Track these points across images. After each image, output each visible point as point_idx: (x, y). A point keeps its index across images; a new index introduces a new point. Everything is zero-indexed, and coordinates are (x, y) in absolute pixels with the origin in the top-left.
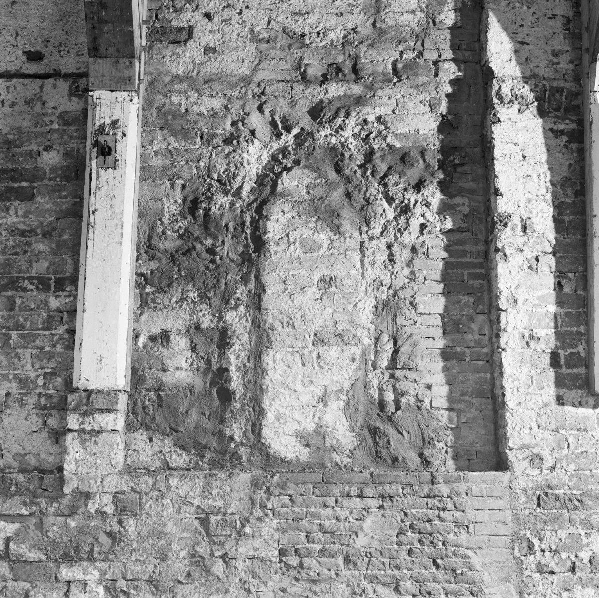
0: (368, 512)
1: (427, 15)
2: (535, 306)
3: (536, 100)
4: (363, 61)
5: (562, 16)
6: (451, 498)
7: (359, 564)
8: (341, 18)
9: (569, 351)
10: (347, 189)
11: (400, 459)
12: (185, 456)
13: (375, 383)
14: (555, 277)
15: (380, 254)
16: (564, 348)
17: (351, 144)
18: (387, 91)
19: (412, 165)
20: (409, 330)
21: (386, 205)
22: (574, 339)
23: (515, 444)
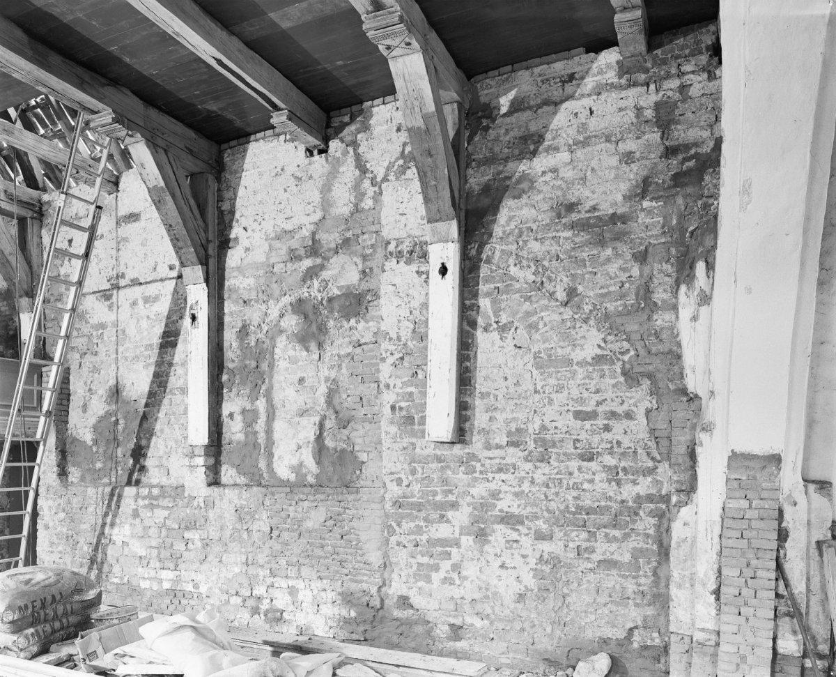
12: (243, 479)
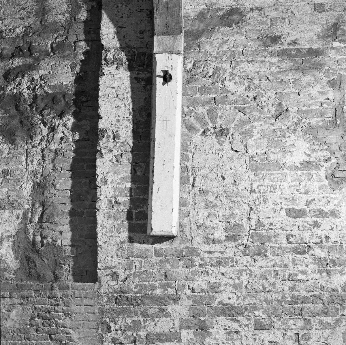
0: (14, 307)
1: (71, 16)
2: (119, 184)
3: (128, 61)
4: (34, 44)
5: (147, 10)
6: (62, 299)
7: (7, 337)
8: (22, 20)
9: (138, 210)
10: (21, 119)
11: (42, 275)
13: (31, 231)
14: (132, 166)
15: (37, 156)
16: (135, 209)
17: (25, 92)
18: (47, 60)
19: (58, 103)
20: (50, 200)
21: (42, 127)
22: (141, 203)
23: (102, 266)
